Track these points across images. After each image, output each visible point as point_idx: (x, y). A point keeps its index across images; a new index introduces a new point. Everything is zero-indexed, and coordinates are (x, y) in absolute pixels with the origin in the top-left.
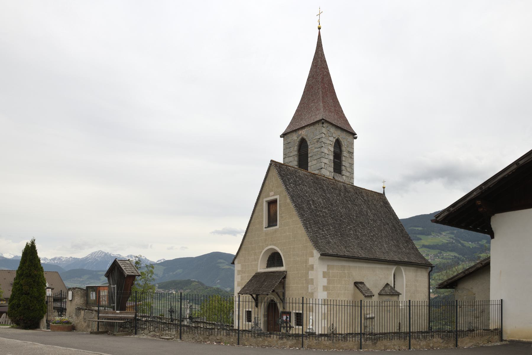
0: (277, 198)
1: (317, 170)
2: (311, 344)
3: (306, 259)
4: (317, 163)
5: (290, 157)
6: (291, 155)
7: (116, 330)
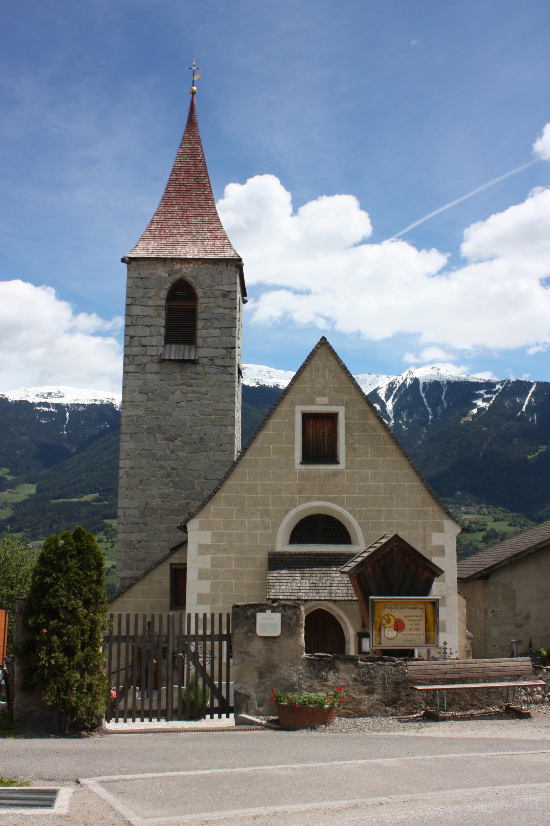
0: (339, 412)
1: (222, 348)
2: (105, 704)
3: (424, 534)
4: (221, 336)
5: (146, 306)
6: (150, 303)
7: (442, 698)
